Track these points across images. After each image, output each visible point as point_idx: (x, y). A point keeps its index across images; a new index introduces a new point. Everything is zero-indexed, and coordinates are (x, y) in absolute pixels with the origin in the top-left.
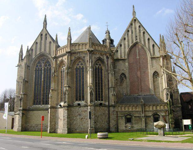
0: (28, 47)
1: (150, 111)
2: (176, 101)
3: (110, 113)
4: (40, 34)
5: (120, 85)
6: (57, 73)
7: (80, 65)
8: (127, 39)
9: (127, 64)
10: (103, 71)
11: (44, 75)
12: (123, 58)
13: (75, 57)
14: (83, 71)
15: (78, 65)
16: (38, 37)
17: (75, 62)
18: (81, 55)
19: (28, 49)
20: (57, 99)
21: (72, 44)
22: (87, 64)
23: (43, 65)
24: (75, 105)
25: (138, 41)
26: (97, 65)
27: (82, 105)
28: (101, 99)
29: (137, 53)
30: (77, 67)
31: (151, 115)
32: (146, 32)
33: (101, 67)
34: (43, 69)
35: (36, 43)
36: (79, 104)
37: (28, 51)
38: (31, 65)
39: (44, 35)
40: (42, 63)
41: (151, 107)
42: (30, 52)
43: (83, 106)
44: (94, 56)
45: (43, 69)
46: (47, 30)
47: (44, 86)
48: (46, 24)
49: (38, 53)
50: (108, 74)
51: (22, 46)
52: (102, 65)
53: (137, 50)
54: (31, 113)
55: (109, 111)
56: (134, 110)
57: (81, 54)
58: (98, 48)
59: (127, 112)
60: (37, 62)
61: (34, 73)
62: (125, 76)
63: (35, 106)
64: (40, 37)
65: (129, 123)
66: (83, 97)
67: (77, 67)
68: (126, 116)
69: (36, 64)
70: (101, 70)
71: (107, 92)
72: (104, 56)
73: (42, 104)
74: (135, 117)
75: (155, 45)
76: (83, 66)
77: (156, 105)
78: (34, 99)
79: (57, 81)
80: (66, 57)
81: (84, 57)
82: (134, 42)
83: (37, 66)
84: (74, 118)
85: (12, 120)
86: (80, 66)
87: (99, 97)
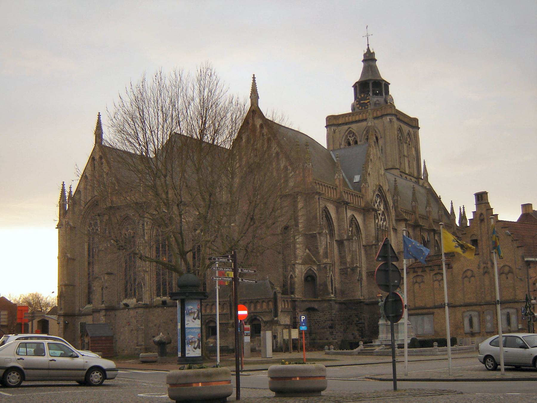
27: (132, 306)
36: (126, 305)
43: (132, 308)
51: (254, 78)
54: (199, 302)
59: (209, 316)
84: (122, 330)
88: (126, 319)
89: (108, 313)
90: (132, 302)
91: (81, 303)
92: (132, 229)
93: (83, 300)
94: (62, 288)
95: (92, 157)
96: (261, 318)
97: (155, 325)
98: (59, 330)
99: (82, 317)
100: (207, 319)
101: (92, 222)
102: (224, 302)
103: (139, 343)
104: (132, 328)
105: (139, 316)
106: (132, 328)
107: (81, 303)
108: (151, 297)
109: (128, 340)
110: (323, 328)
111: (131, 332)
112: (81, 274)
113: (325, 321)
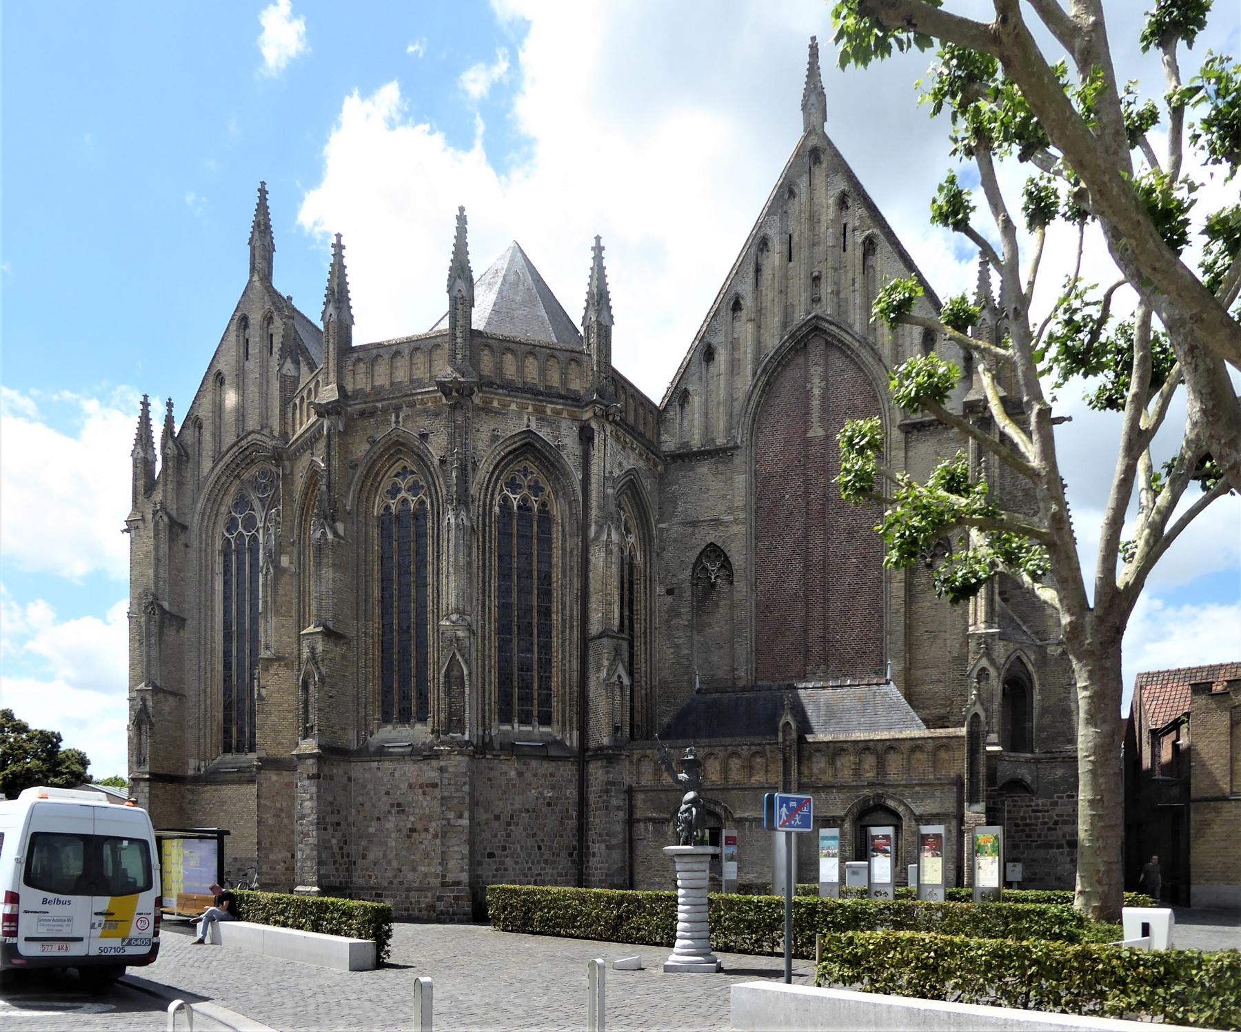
0: (170, 405)
1: (841, 788)
2: (1047, 719)
3: (592, 798)
5: (690, 626)
10: (557, 534)
12: (720, 441)
13: (373, 442)
14: (421, 535)
15: (395, 491)
17: (372, 474)
21: (375, 352)
25: (827, 309)
26: (513, 485)
29: (816, 403)
30: (388, 508)
31: (842, 814)
32: (881, 239)
33: (544, 505)
35: (215, 378)
38: (194, 521)
39: (255, 318)
49: (229, 439)
53: (816, 380)
57: (407, 417)
58: (521, 369)
60: (229, 500)
61: (219, 568)
62: (726, 564)
63: (229, 757)
70: (545, 518)
72: (564, 424)
73: (233, 751)
76: (422, 503)
79: (295, 607)
81: (424, 436)
82: (800, 316)
83: (231, 525)
84: (372, 830)
87: (525, 699)
88: (388, 793)
89: (326, 770)
91: (202, 748)
92: (414, 489)
93: (208, 741)
94: (144, 700)
95: (238, 314)
96: (905, 805)
97: (497, 818)
101: (238, 516)
107: (202, 748)
108: (484, 724)
109: (395, 864)
110: (1049, 846)
111: (409, 837)
112: (202, 664)
113: (1056, 823)
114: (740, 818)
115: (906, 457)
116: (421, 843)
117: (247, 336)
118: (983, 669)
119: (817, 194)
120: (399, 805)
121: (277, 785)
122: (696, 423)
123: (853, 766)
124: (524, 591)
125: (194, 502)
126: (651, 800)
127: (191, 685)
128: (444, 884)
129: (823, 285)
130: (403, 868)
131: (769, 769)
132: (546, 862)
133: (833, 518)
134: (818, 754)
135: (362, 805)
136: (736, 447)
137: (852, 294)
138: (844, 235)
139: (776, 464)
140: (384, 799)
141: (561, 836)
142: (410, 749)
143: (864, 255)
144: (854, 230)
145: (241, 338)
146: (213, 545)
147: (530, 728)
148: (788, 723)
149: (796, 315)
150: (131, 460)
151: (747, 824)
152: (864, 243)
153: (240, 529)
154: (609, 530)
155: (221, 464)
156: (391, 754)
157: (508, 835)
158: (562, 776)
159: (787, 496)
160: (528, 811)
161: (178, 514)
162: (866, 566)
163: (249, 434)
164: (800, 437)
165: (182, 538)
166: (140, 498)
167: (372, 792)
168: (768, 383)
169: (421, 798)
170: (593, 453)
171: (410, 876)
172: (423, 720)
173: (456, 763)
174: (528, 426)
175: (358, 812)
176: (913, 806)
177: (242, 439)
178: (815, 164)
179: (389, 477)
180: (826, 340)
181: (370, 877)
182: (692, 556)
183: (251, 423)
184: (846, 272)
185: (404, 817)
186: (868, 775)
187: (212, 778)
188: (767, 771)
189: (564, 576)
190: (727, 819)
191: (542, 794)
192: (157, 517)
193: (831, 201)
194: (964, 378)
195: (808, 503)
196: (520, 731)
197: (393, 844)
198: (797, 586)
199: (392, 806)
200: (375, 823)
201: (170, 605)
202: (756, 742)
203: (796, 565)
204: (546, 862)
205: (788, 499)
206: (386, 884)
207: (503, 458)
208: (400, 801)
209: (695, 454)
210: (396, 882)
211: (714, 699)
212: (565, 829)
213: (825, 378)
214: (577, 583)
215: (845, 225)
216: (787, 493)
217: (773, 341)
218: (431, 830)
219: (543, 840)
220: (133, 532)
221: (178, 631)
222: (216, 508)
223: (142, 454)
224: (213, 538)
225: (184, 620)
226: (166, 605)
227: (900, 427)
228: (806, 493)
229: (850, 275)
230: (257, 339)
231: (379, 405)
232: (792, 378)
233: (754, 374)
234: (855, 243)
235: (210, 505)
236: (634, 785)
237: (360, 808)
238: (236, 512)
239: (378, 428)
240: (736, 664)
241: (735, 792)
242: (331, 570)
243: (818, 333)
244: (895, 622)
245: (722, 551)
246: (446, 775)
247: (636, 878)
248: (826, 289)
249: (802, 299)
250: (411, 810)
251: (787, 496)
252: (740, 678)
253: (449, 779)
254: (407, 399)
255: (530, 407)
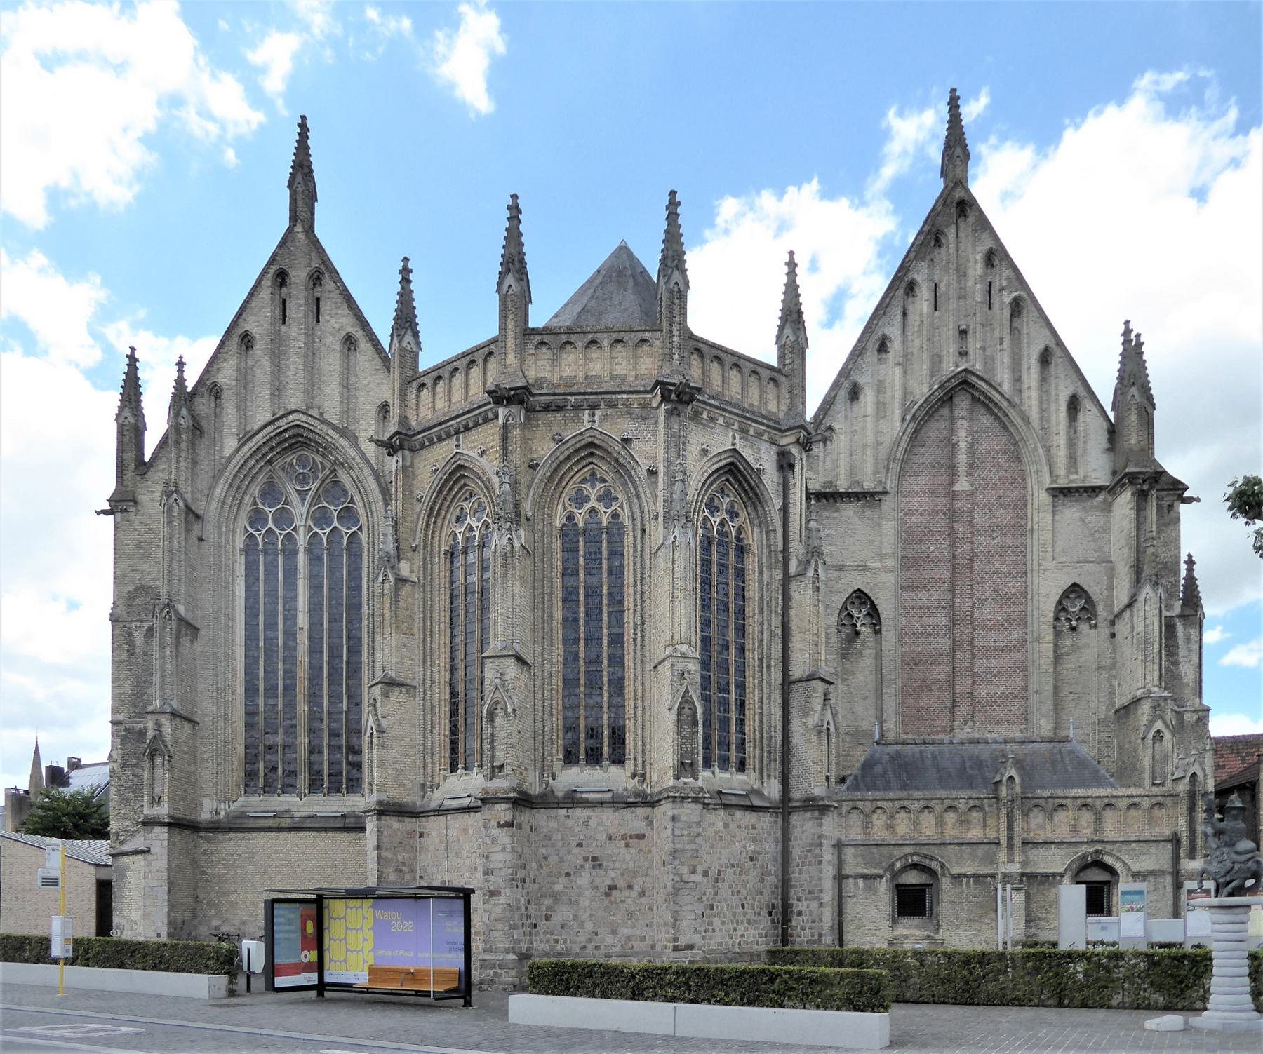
0: (181, 364)
4: (264, 272)
6: (418, 562)
7: (593, 503)
8: (895, 346)
9: (889, 528)
10: (751, 565)
11: (315, 588)
12: (868, 485)
13: (559, 440)
15: (580, 499)
16: (252, 294)
18: (607, 428)
19: (180, 382)
20: (426, 753)
22: (646, 495)
23: (300, 511)
24: (560, 794)
28: (733, 755)
29: (962, 458)
30: (571, 518)
31: (1061, 870)
34: (302, 540)
37: (182, 399)
39: (299, 275)
40: (295, 498)
41: (879, 820)
42: (203, 405)
44: (697, 438)
45: (302, 540)
46: (315, 244)
47: (311, 667)
48: (312, 196)
50: (787, 579)
52: (743, 515)
55: (786, 838)
56: (951, 832)
59: (908, 850)
61: (240, 569)
62: (874, 613)
63: (254, 799)
64: (265, 294)
65: (915, 921)
66: (618, 737)
67: (571, 518)
68: (895, 875)
69: (248, 499)
70: (742, 550)
71: (777, 709)
74: (957, 877)
75: (1087, 404)
76: (615, 515)
77: (1098, 802)
78: (250, 759)
79: (418, 624)
80: (489, 435)
82: (950, 367)
83: (257, 518)
85: (94, 889)
86: (593, 511)
88: (580, 845)
90: (470, 783)
95: (274, 268)
96: (1123, 861)
98: (145, 877)
99: (232, 835)
100: (900, 859)
101: (267, 509)
102: (972, 803)
103: (682, 941)
104: (613, 879)
105: (685, 833)
106: (613, 879)
109: (589, 926)
111: (607, 895)
114: (959, 875)
115: (1053, 520)
116: (623, 901)
117: (283, 296)
118: (1158, 731)
119: (962, 248)
120: (594, 859)
121: (399, 833)
122: (842, 463)
123: (1072, 822)
124: (724, 626)
125: (211, 488)
126: (863, 855)
127: (205, 710)
128: (676, 949)
129: (970, 340)
130: (599, 931)
131: (988, 823)
132: (749, 921)
133: (979, 574)
134: (1036, 810)
135: (546, 858)
136: (885, 493)
137: (999, 353)
138: (990, 292)
139: (921, 514)
140: (576, 851)
141: (762, 893)
142: (610, 795)
143: (1011, 315)
144: (1002, 289)
145: (277, 297)
146: (234, 541)
147: (728, 776)
148: (1011, 777)
149: (944, 365)
150: (114, 427)
151: (965, 880)
152: (1011, 303)
153: (270, 525)
154: (816, 566)
155: (250, 444)
156: (587, 801)
157: (716, 893)
158: (762, 828)
159: (932, 548)
160: (733, 866)
161: (193, 499)
162: (1011, 624)
163: (291, 413)
164: (944, 489)
165: (196, 528)
166: (129, 474)
167: (560, 844)
168: (916, 432)
169: (623, 850)
170: (793, 482)
171: (609, 940)
172: (618, 760)
173: (689, 811)
174: (733, 444)
175: (541, 866)
176: (1129, 862)
177: (281, 418)
178: (960, 216)
179: (575, 483)
180: (972, 395)
181: (556, 941)
182: (838, 601)
183: (292, 400)
184: (993, 330)
185: (602, 872)
186: (1085, 831)
187: (238, 825)
188: (985, 826)
189: (761, 610)
190: (943, 874)
191: (745, 848)
192: (172, 500)
193: (979, 257)
194: (1108, 449)
195: (954, 557)
196: (721, 778)
197: (587, 903)
198: (943, 640)
199: (586, 859)
200: (563, 880)
201: (186, 610)
202: (974, 796)
203: (941, 618)
204: (749, 921)
205: (933, 551)
206: (578, 950)
207: (711, 475)
208: (597, 854)
209: (841, 495)
210: (590, 946)
211: (897, 751)
212: (765, 886)
213: (970, 434)
214: (776, 621)
215: (990, 283)
216: (932, 545)
217: (922, 391)
218: (636, 887)
219: (746, 898)
220: (119, 515)
221: (192, 642)
222: (239, 496)
223: (132, 420)
224: (234, 532)
225: (197, 629)
226: (181, 609)
227: (1048, 489)
228: (953, 546)
229: (997, 333)
230: (302, 302)
231: (572, 399)
232: (938, 429)
233: (903, 419)
234: (1002, 303)
235: (232, 493)
236: (843, 838)
237: (543, 863)
238: (263, 504)
239: (566, 425)
240: (884, 715)
241: (952, 846)
242: (518, 583)
243: (965, 386)
244: (1042, 681)
245: (869, 598)
246: (678, 825)
247: (844, 937)
248: (973, 344)
249: (951, 350)
250: (611, 864)
251: (932, 548)
252: (889, 730)
253: (682, 829)
254: (609, 396)
255: (736, 423)
